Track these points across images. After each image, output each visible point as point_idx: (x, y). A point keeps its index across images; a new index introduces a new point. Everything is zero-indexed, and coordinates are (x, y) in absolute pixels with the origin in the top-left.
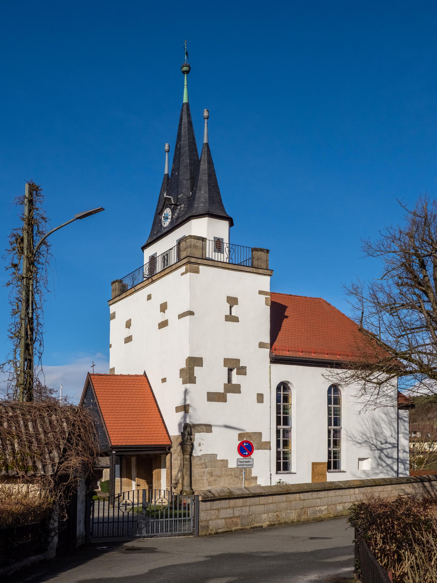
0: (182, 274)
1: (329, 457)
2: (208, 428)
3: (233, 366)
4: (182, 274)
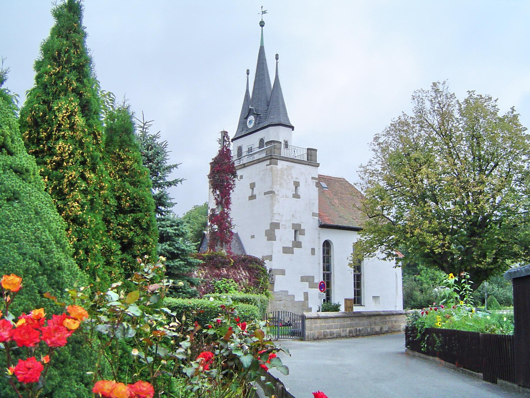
0: (267, 165)
1: (355, 296)
2: (283, 272)
3: (298, 230)
4: (267, 165)
